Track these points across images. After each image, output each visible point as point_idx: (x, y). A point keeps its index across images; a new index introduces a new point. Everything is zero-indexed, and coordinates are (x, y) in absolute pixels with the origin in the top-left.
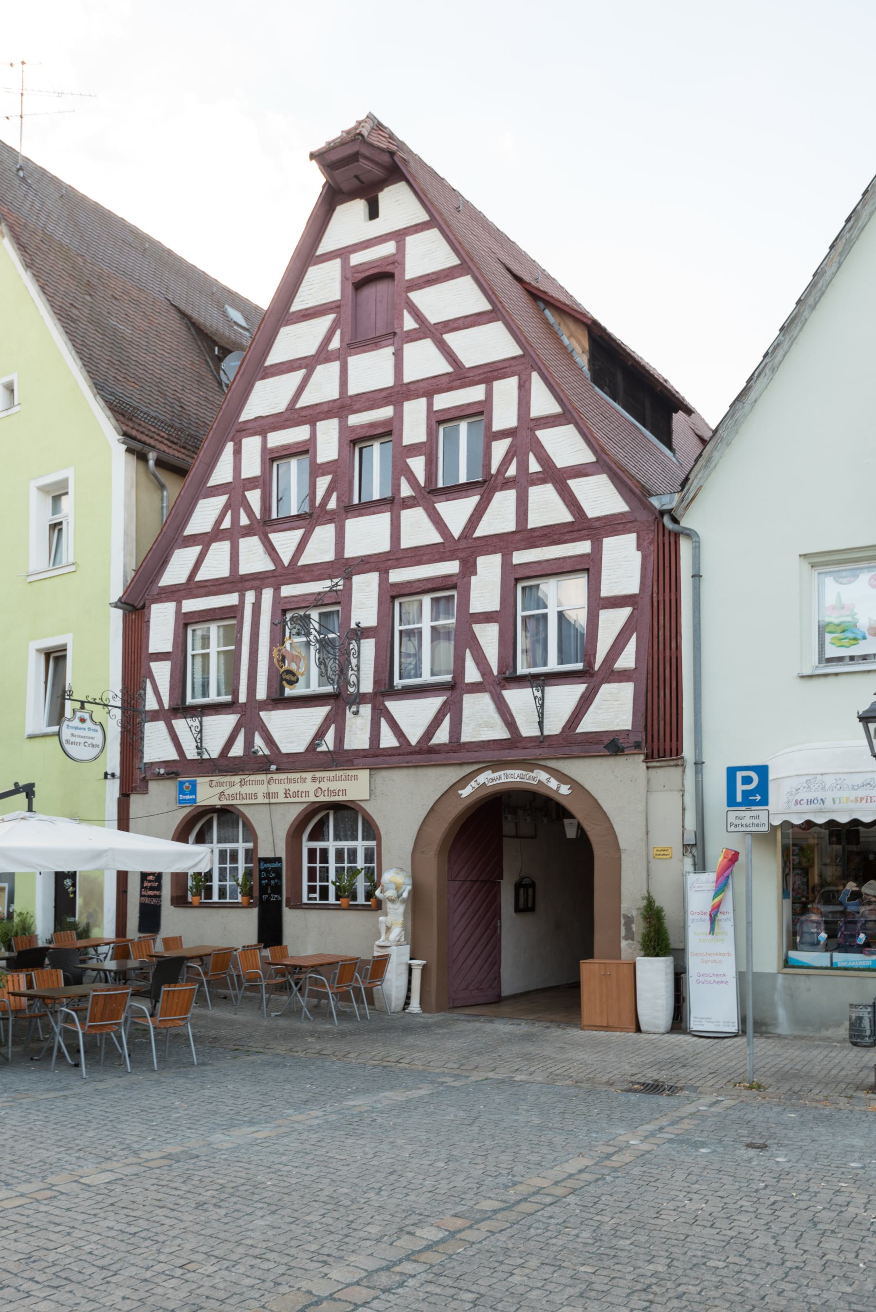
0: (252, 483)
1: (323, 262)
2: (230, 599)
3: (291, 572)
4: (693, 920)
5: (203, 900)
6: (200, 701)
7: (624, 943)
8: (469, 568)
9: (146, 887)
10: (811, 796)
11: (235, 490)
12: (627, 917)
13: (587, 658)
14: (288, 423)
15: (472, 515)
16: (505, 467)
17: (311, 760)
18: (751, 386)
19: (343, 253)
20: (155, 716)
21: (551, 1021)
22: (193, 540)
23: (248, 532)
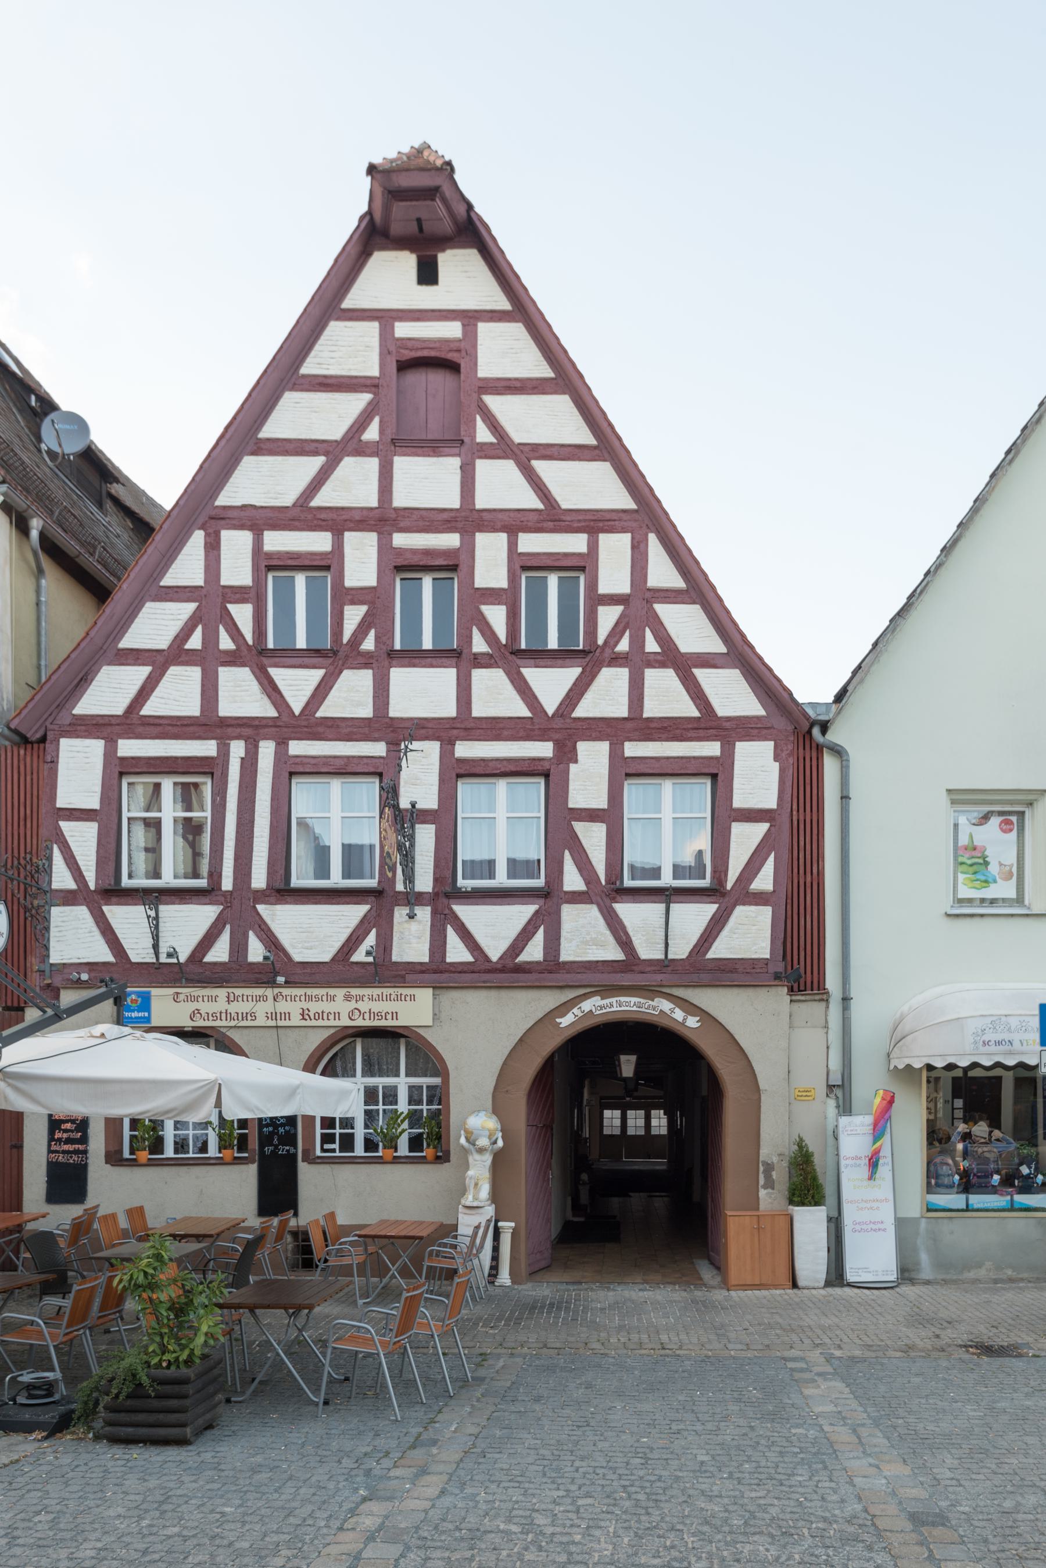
0: (239, 594)
1: (351, 319)
2: (207, 748)
3: (305, 723)
4: (847, 1166)
5: (236, 1155)
6: (142, 882)
7: (762, 1193)
8: (566, 754)
9: (59, 1140)
10: (999, 1037)
11: (212, 601)
12: (765, 1164)
13: (717, 875)
14: (297, 523)
15: (571, 690)
16: (615, 639)
17: (339, 971)
18: (913, 603)
19: (385, 318)
20: (69, 898)
21: (646, 1282)
22: (135, 657)
23: (233, 659)
